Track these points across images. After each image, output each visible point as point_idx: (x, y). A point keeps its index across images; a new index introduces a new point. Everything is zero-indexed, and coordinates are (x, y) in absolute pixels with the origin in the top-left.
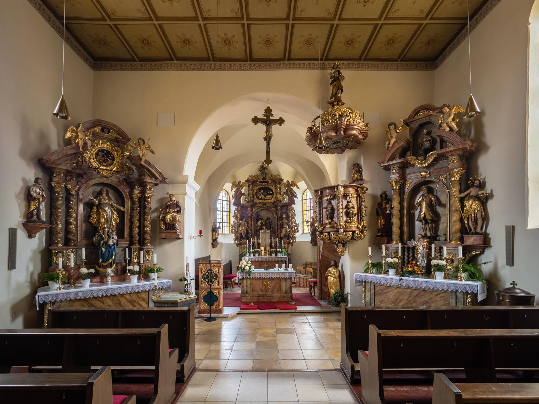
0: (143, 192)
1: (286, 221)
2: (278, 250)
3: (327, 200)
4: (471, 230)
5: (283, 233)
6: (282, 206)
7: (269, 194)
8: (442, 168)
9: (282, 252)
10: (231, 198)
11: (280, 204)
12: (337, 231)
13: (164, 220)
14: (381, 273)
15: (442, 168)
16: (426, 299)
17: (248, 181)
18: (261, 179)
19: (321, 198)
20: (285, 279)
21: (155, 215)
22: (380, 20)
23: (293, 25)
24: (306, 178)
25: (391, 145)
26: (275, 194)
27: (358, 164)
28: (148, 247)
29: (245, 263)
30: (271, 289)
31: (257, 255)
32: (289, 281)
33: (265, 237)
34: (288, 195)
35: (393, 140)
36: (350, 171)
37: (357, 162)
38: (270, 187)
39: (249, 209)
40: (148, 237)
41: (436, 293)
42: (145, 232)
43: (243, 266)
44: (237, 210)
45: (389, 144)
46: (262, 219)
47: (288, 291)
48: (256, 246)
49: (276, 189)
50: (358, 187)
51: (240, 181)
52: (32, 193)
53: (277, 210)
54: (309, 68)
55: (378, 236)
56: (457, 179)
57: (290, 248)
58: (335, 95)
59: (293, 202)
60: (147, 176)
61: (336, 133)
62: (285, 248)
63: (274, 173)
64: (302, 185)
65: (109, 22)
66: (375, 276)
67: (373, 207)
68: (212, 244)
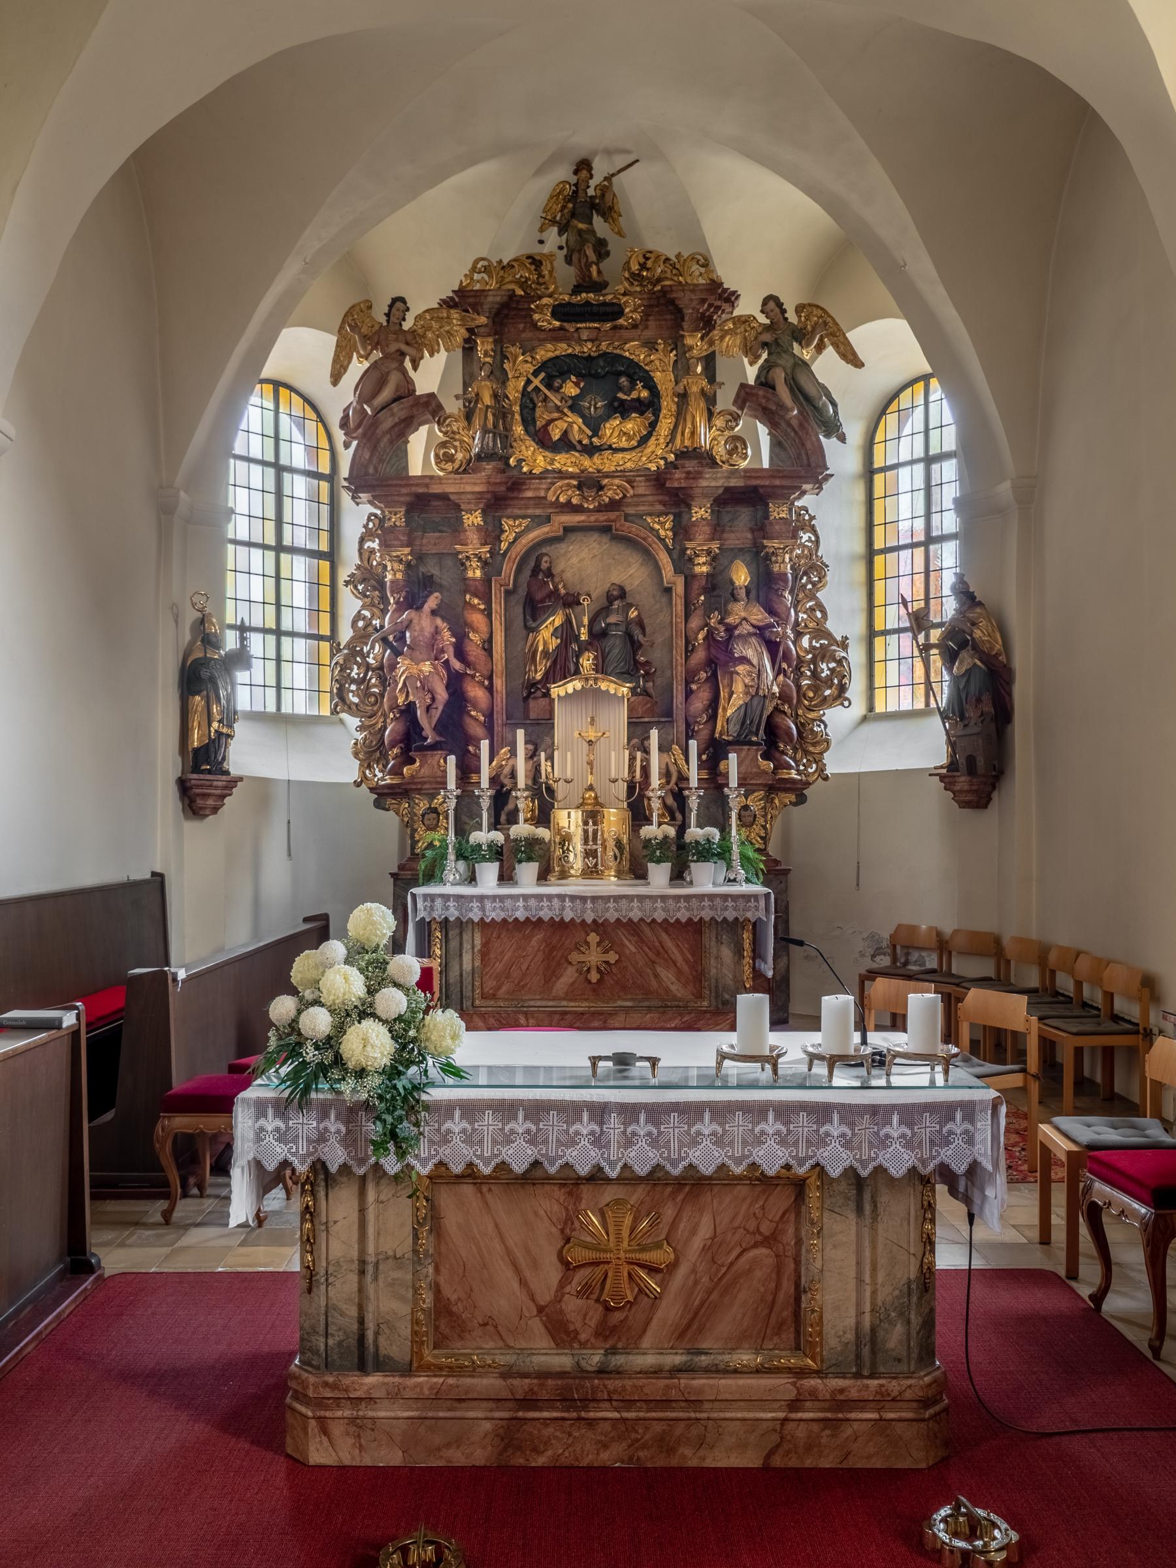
1: (758, 615)
2: (695, 832)
5: (733, 706)
6: (729, 499)
7: (623, 410)
9: (722, 854)
10: (339, 436)
11: (713, 481)
24: (922, 267)
26: (668, 405)
29: (347, 983)
30: (669, 1312)
31: (527, 872)
33: (591, 739)
34: (772, 416)
38: (634, 351)
39: (473, 519)
43: (318, 1022)
44: (379, 529)
46: (571, 601)
47: (895, 1337)
48: (523, 802)
49: (682, 368)
51: (398, 303)
53: (682, 531)
64: (888, 345)
68: (184, 786)
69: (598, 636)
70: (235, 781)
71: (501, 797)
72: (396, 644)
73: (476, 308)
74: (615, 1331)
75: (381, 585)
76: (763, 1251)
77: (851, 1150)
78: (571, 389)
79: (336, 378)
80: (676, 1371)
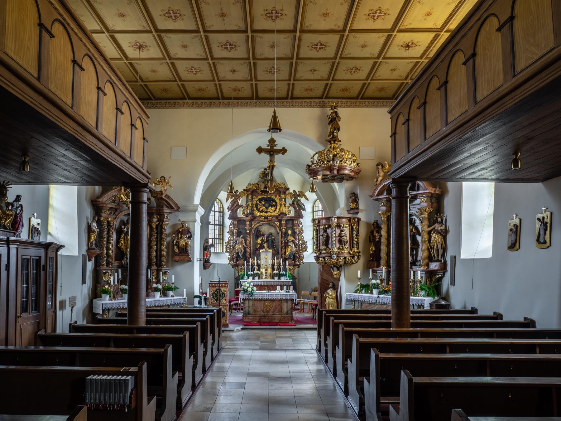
0: (161, 220)
1: (292, 238)
2: (281, 272)
3: (323, 229)
4: (435, 258)
5: (288, 253)
6: (287, 220)
7: (272, 206)
9: (286, 275)
11: (285, 218)
12: (331, 257)
13: (178, 244)
14: (368, 293)
17: (246, 190)
18: (262, 186)
19: (319, 226)
20: (286, 300)
21: (168, 239)
22: (367, 80)
23: (293, 84)
25: (378, 183)
26: (278, 205)
27: (354, 194)
28: (165, 268)
29: (248, 285)
30: (272, 310)
31: (257, 278)
32: (289, 303)
33: (266, 257)
35: (380, 178)
36: (347, 199)
37: (354, 192)
38: (273, 197)
39: (248, 223)
40: (164, 259)
42: (161, 256)
43: (246, 288)
44: (232, 224)
45: (377, 181)
46: (263, 235)
47: (289, 312)
49: (281, 200)
50: (350, 218)
52: (92, 227)
53: (281, 224)
54: (310, 106)
55: (370, 261)
56: (426, 216)
57: (296, 270)
58: (332, 133)
59: (301, 216)
60: (164, 206)
61: (330, 172)
62: (290, 270)
63: (279, 181)
65: (141, 83)
66: (363, 296)
67: (367, 234)
69: (267, 241)
70: (211, 264)
71: (253, 266)
72: (236, 243)
73: (248, 191)
74: (268, 312)
75: (233, 233)
78: (263, 203)
79: (227, 201)
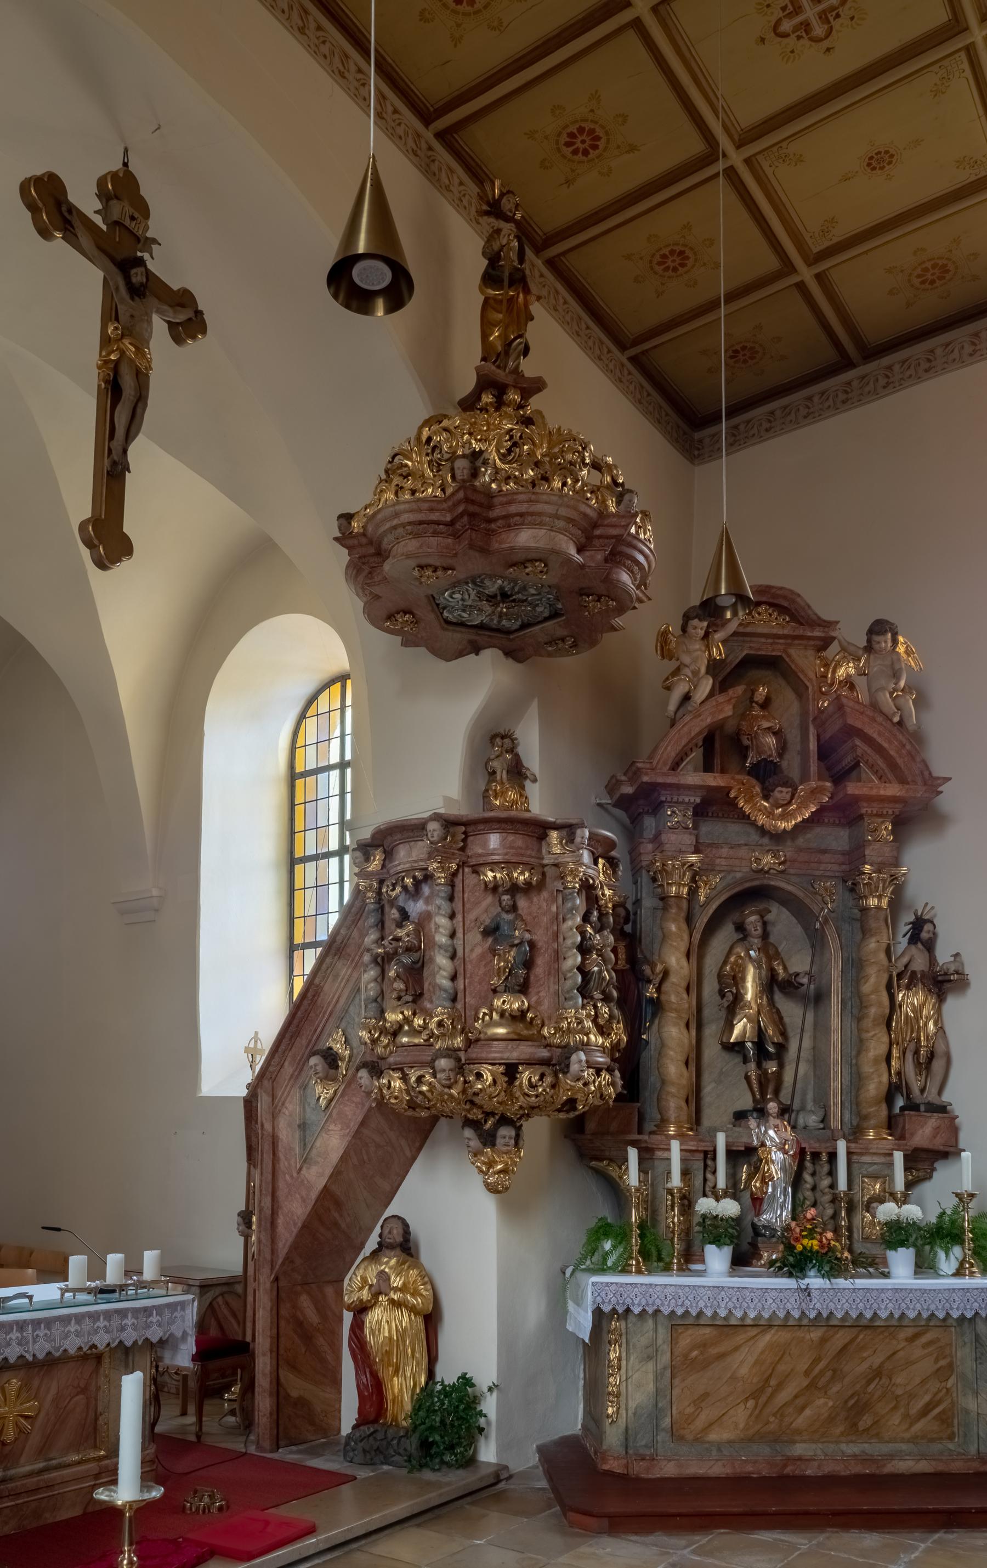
8: (824, 852)
15: (824, 852)
16: (877, 1360)
41: (910, 1332)
76: (81, 1396)
77: (22, 1345)
80: (41, 1472)
